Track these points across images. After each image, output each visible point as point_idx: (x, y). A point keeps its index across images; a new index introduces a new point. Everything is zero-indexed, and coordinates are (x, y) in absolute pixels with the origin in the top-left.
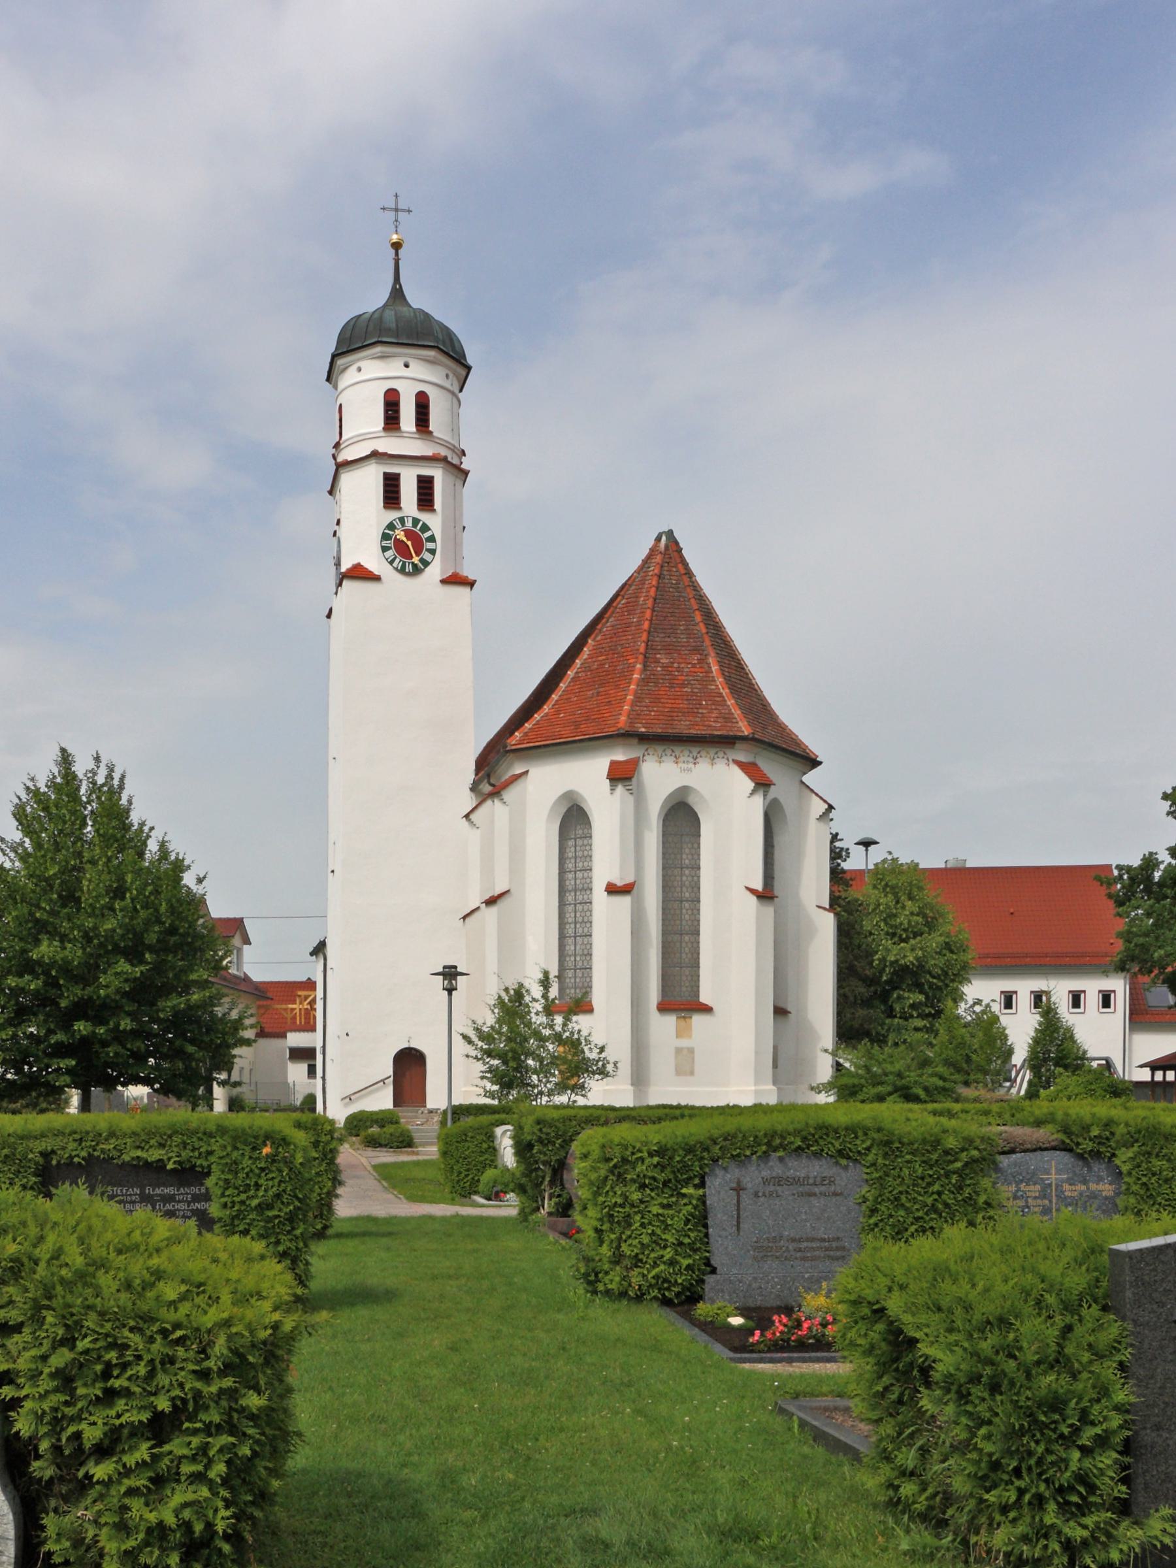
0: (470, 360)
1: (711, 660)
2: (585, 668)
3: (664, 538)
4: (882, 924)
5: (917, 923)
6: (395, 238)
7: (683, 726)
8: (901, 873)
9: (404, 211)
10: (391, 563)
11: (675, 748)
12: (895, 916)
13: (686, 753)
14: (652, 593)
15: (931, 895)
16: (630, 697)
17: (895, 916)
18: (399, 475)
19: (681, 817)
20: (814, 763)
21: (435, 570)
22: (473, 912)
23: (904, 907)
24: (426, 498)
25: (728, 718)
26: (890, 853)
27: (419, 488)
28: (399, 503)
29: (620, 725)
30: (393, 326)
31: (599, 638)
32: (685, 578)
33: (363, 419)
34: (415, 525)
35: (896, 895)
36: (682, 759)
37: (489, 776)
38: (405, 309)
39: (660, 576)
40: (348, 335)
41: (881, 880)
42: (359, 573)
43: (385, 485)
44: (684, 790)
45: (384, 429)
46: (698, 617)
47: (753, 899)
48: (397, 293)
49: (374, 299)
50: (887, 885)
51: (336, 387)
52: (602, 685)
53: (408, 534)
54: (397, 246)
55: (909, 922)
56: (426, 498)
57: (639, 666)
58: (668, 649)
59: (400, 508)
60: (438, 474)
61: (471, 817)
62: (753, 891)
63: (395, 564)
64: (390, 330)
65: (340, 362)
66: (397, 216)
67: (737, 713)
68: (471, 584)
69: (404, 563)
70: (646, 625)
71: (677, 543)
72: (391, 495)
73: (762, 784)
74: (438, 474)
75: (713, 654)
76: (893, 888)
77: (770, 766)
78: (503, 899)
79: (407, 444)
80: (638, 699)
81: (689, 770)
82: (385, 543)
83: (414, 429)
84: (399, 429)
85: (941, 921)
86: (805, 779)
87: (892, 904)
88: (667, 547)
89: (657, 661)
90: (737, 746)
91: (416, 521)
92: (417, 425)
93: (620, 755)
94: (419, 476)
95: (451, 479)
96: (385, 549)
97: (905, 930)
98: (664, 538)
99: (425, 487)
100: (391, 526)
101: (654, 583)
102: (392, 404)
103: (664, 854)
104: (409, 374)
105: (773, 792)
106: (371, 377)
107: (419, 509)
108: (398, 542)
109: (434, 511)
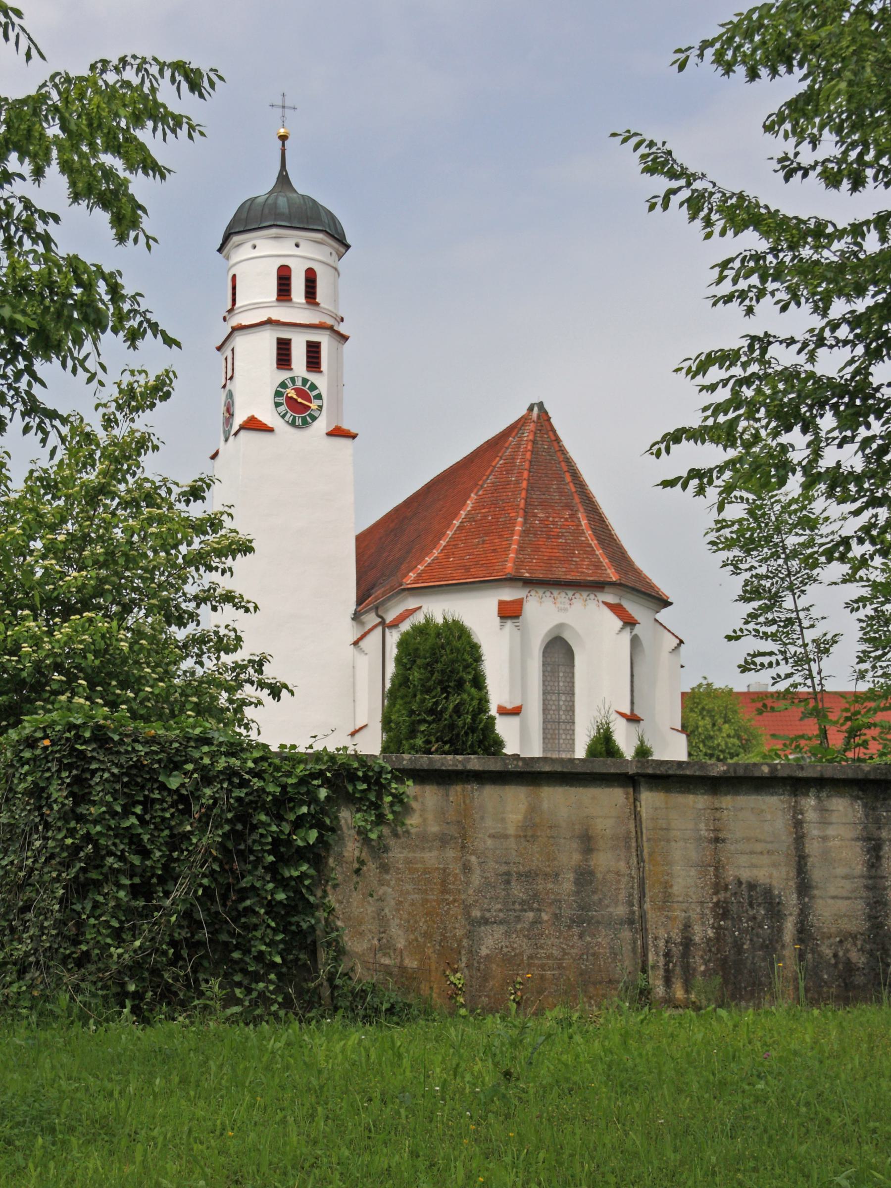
0: (349, 241)
1: (580, 515)
2: (470, 517)
3: (536, 409)
4: (701, 746)
5: (734, 745)
6: (282, 131)
7: (560, 573)
8: (716, 697)
9: (290, 108)
10: (283, 417)
12: (711, 738)
13: (563, 595)
14: (528, 455)
15: (746, 716)
16: (514, 546)
17: (711, 738)
19: (559, 652)
20: (666, 603)
21: (321, 425)
22: (361, 729)
23: (720, 730)
25: (598, 566)
26: (705, 678)
27: (308, 352)
28: (290, 365)
29: (507, 571)
30: (286, 211)
31: (480, 493)
32: (555, 443)
33: (257, 292)
35: (712, 717)
36: (559, 600)
37: (377, 608)
38: (295, 195)
39: (534, 442)
40: (244, 216)
41: (698, 704)
42: (253, 425)
43: (278, 349)
44: (561, 626)
45: (278, 300)
46: (568, 478)
47: (624, 721)
48: (283, 180)
49: (262, 186)
50: (703, 709)
51: (227, 258)
52: (487, 534)
53: (299, 391)
54: (283, 138)
55: (726, 743)
57: (520, 519)
58: (544, 505)
60: (324, 339)
61: (361, 644)
62: (623, 715)
63: (287, 418)
65: (236, 239)
66: (283, 112)
67: (605, 561)
68: (354, 437)
70: (524, 484)
71: (546, 413)
72: (284, 357)
73: (629, 622)
74: (324, 339)
75: (582, 510)
76: (709, 711)
77: (634, 608)
79: (296, 312)
80: (521, 549)
81: (566, 610)
82: (278, 400)
83: (303, 301)
84: (290, 300)
85: (754, 742)
86: (658, 616)
87: (709, 727)
88: (539, 417)
89: (535, 515)
90: (606, 590)
91: (305, 381)
92: (306, 297)
93: (508, 594)
94: (308, 342)
95: (335, 343)
96: (277, 405)
97: (722, 751)
98: (536, 409)
100: (283, 385)
101: (529, 447)
103: (544, 681)
104: (300, 252)
105: (638, 630)
108: (290, 399)
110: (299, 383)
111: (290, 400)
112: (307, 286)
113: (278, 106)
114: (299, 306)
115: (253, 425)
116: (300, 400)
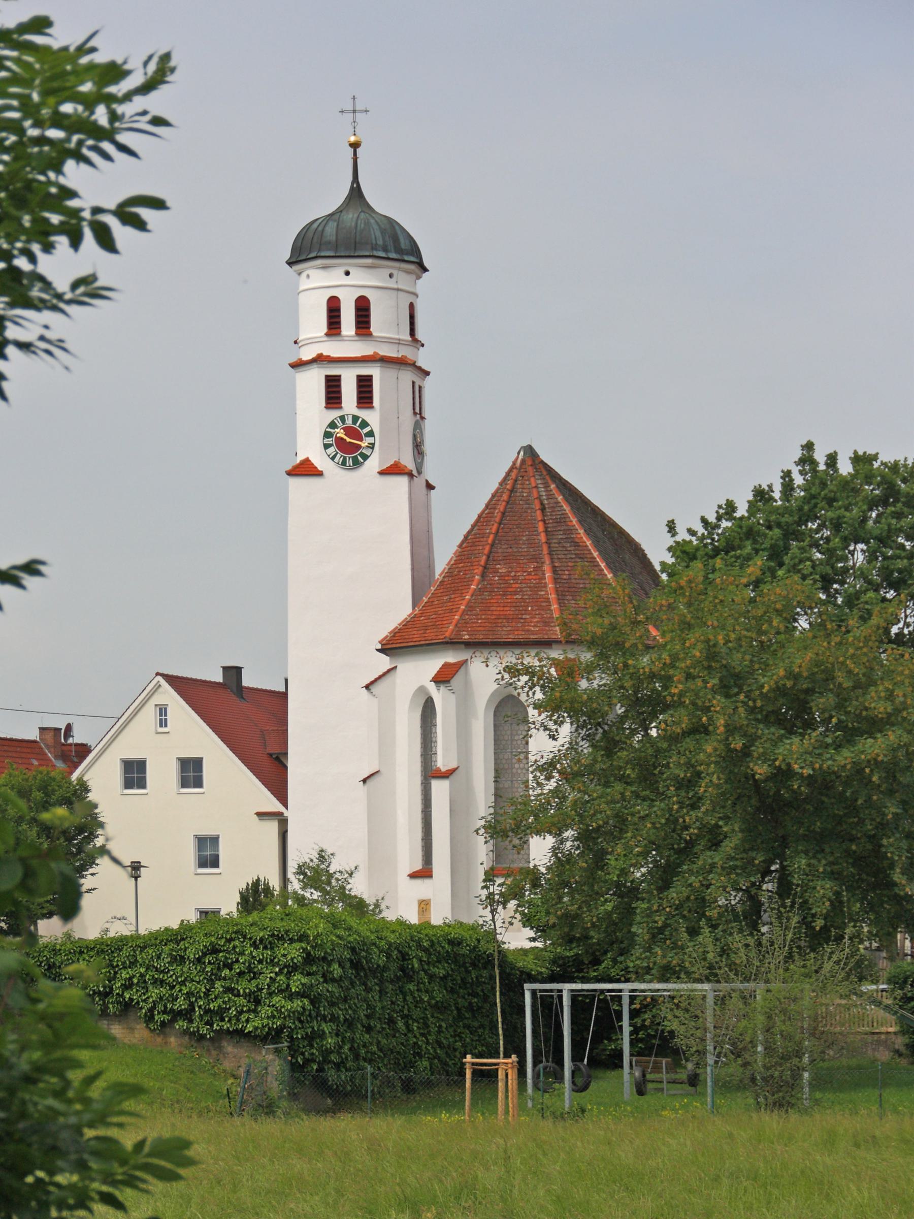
6: (353, 139)
7: (504, 633)
9: (361, 111)
10: (333, 458)
11: (499, 651)
18: (340, 376)
21: (374, 463)
24: (365, 395)
28: (340, 403)
34: (354, 422)
42: (306, 469)
48: (356, 193)
53: (349, 431)
54: (355, 146)
56: (365, 395)
59: (341, 408)
63: (336, 460)
64: (329, 243)
66: (354, 118)
69: (345, 458)
72: (333, 395)
78: (373, 778)
79: (348, 345)
80: (470, 607)
89: (496, 571)
90: (554, 646)
91: (355, 418)
93: (451, 657)
96: (326, 446)
99: (365, 386)
100: (333, 425)
102: (334, 309)
106: (322, 282)
107: (358, 407)
108: (339, 441)
109: (372, 407)
110: (349, 422)
111: (340, 442)
112: (368, 316)
113: (348, 111)
114: (349, 339)
115: (306, 469)
116: (348, 440)
